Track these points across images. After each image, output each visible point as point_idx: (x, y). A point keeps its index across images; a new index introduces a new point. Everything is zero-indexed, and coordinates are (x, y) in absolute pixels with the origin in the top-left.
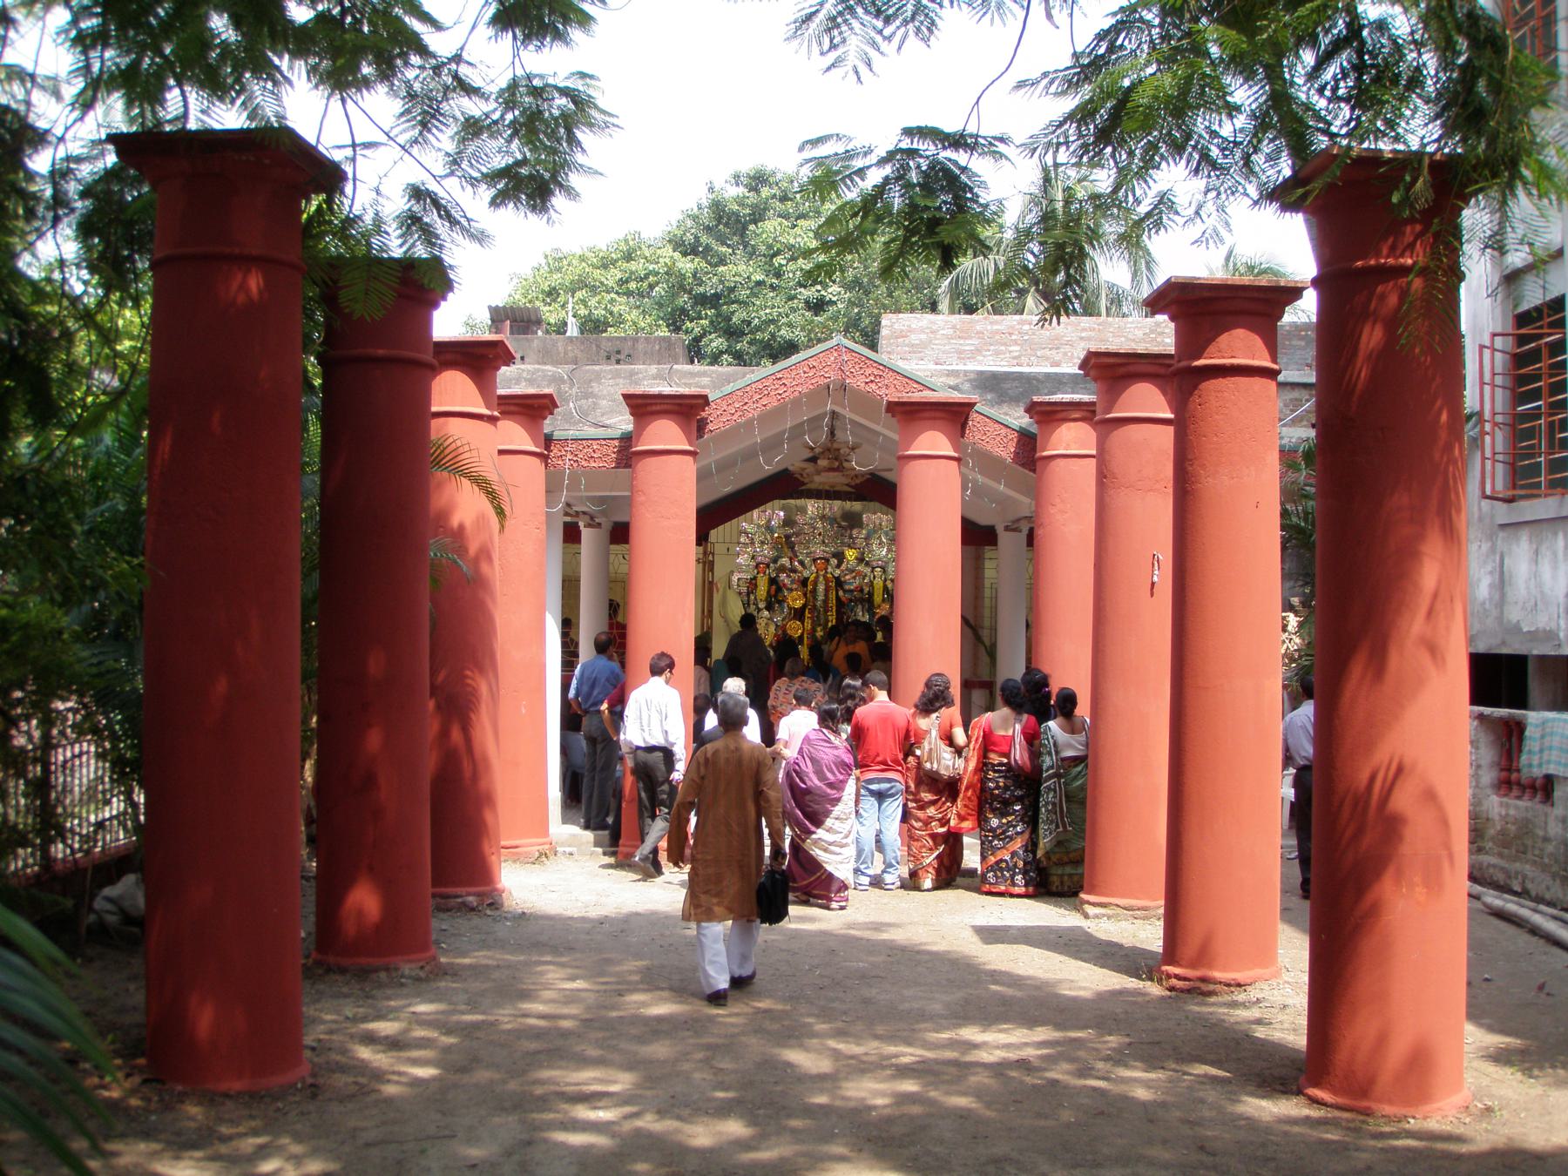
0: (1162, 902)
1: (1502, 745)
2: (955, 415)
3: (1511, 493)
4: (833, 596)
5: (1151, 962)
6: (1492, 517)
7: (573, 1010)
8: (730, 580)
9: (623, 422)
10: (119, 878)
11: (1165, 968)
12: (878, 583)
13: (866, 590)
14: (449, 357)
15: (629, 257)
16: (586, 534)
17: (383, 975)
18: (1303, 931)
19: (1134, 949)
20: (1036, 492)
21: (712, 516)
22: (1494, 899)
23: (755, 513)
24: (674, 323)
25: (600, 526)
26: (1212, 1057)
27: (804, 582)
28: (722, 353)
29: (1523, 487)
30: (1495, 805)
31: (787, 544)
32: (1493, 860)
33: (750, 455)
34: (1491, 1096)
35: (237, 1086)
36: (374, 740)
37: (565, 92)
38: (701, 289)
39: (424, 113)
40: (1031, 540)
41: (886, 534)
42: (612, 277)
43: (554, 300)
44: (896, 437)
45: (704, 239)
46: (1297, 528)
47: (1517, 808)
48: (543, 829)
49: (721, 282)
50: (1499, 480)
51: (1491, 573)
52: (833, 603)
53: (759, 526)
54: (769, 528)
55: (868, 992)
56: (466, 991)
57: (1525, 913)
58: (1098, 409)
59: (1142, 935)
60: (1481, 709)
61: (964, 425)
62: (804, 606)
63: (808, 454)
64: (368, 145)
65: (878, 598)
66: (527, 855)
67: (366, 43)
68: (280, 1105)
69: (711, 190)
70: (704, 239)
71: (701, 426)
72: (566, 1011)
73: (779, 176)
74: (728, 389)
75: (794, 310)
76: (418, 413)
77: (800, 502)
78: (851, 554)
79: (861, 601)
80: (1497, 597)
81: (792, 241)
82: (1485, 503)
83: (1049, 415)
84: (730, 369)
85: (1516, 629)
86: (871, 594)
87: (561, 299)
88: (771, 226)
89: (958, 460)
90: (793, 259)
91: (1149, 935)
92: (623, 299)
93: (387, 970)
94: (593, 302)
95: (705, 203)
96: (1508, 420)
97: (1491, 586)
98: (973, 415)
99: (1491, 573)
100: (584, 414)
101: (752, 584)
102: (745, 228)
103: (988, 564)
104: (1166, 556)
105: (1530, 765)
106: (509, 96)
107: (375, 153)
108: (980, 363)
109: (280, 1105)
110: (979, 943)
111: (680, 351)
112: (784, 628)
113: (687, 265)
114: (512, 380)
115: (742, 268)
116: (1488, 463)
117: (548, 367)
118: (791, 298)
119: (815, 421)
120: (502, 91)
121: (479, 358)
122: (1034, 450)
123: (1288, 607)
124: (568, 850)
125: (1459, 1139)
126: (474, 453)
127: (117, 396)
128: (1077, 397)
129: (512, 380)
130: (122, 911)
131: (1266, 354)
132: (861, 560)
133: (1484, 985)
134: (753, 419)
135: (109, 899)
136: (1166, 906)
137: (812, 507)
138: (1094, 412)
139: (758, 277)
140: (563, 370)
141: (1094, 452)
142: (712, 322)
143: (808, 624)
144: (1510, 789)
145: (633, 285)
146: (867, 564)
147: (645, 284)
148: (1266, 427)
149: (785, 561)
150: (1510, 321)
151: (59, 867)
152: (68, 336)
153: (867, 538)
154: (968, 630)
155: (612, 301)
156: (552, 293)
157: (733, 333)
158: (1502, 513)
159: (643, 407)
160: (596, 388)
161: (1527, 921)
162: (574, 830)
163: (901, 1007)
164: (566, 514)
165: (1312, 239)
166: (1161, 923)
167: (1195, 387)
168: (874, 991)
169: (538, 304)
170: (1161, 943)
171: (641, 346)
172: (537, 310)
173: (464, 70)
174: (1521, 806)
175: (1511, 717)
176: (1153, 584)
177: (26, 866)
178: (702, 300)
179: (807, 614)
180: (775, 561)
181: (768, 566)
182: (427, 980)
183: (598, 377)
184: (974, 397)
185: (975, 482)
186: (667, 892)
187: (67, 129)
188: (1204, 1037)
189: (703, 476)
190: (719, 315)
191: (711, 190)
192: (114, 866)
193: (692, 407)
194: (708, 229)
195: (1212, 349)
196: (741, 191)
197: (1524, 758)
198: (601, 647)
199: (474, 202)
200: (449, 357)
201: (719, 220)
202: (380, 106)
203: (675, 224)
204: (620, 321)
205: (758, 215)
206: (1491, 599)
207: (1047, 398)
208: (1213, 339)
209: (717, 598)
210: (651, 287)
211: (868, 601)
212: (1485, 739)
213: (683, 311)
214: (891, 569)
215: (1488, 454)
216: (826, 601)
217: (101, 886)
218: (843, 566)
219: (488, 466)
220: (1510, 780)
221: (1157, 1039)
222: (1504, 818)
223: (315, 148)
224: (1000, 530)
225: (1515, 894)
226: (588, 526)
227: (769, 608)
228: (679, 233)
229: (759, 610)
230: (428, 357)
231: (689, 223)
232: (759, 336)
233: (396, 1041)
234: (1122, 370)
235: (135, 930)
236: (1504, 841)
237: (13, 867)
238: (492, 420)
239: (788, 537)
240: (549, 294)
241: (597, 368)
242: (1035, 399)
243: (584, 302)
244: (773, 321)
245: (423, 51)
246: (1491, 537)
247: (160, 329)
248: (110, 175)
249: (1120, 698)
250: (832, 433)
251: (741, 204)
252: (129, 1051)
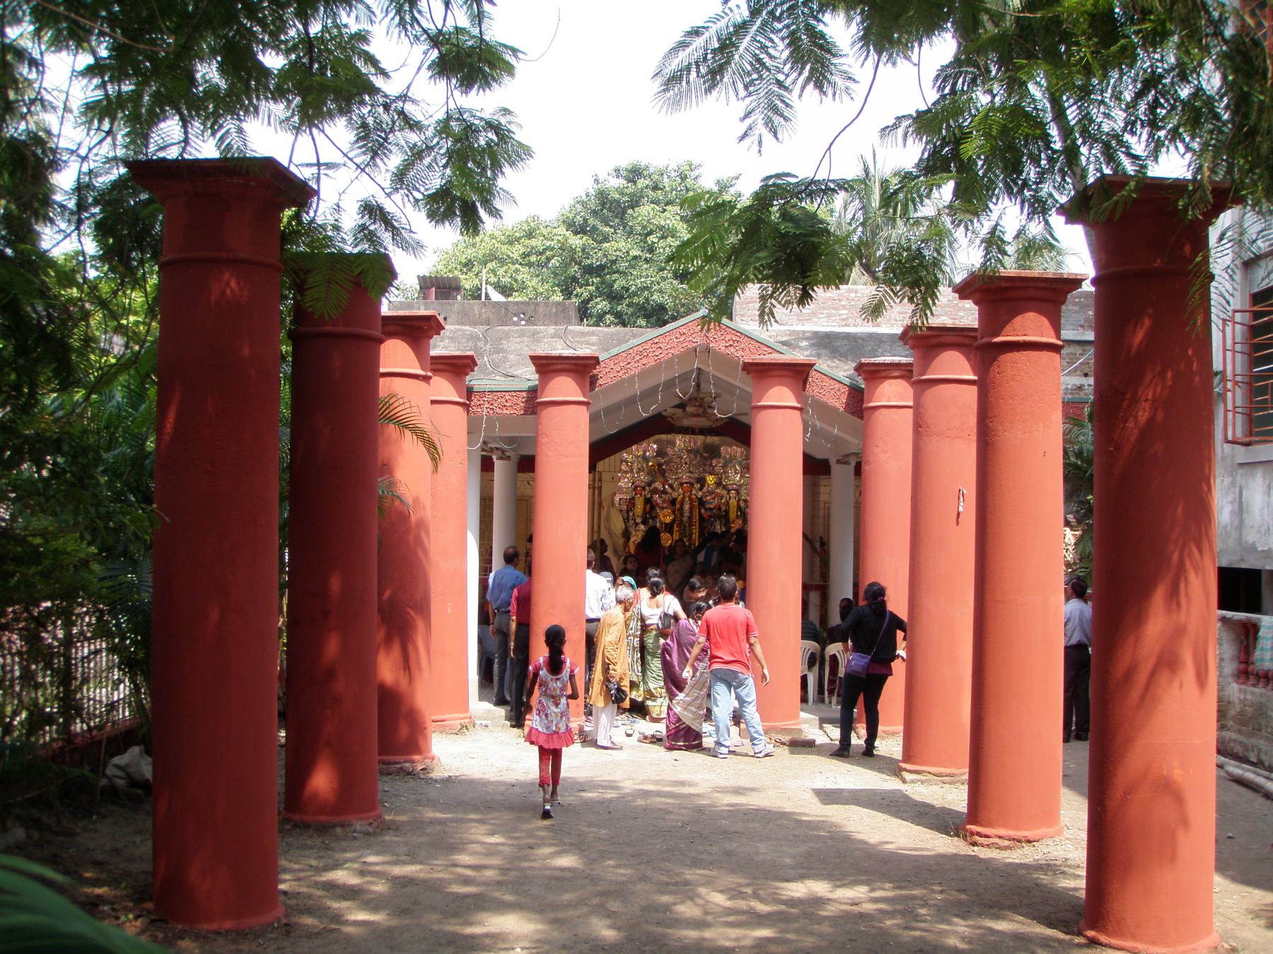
0: (967, 770)
1: (1241, 642)
2: (798, 374)
3: (1248, 439)
4: (696, 513)
5: (957, 821)
6: (1233, 457)
7: (494, 861)
8: (613, 501)
9: (529, 375)
10: (125, 750)
11: (969, 827)
12: (733, 502)
13: (723, 508)
14: (392, 328)
15: (530, 235)
16: (498, 465)
17: (339, 830)
18: (1082, 794)
19: (943, 809)
20: (864, 435)
21: (601, 450)
22: (1235, 769)
23: (634, 447)
24: (567, 288)
25: (511, 461)
26: (1009, 903)
27: (673, 502)
28: (605, 313)
29: (1258, 434)
30: (1235, 690)
31: (659, 471)
32: (1234, 736)
33: (631, 401)
34: (1235, 938)
35: (228, 924)
36: (332, 646)
37: (490, 125)
38: (589, 261)
39: (372, 142)
40: (858, 470)
41: (740, 464)
42: (517, 251)
43: (470, 270)
44: (750, 390)
45: (592, 221)
46: (1075, 466)
47: (1252, 693)
48: (465, 708)
49: (605, 256)
50: (1237, 427)
51: (1231, 502)
52: (696, 518)
53: (638, 457)
54: (644, 457)
55: (732, 846)
56: (406, 844)
57: (1260, 780)
58: (915, 370)
59: (950, 797)
60: (1224, 612)
61: (805, 382)
62: (673, 521)
63: (677, 402)
64: (330, 166)
65: (732, 515)
66: (451, 727)
67: (330, 84)
68: (261, 941)
69: (597, 181)
70: (592, 221)
71: (593, 381)
72: (487, 862)
73: (652, 170)
74: (615, 351)
75: (664, 279)
76: (369, 374)
77: (670, 437)
78: (711, 479)
79: (720, 517)
80: (1237, 522)
81: (663, 223)
82: (1226, 446)
83: (874, 373)
84: (613, 329)
85: (1252, 549)
86: (727, 512)
87: (476, 269)
88: (645, 210)
89: (800, 409)
90: (663, 237)
91: (956, 798)
92: (526, 269)
93: (342, 826)
94: (501, 272)
95: (592, 192)
96: (1246, 380)
97: (1232, 513)
98: (813, 373)
99: (1231, 502)
100: (496, 366)
101: (631, 503)
102: (624, 212)
103: (822, 490)
104: (970, 491)
105: (1262, 660)
106: (444, 128)
107: (339, 176)
108: (815, 324)
109: (261, 941)
110: (819, 804)
111: (573, 314)
113: (576, 241)
114: (440, 347)
115: (622, 244)
116: (1230, 415)
117: (467, 328)
118: (662, 269)
119: (684, 377)
120: (439, 122)
121: (417, 330)
122: (862, 401)
123: (1067, 524)
124: (484, 722)
126: (414, 410)
127: (124, 365)
128: (897, 359)
129: (440, 347)
130: (129, 777)
131: (1052, 332)
132: (719, 484)
133: (1228, 842)
134: (634, 376)
135: (117, 766)
136: (970, 773)
137: (680, 441)
138: (911, 371)
139: (635, 252)
140: (478, 330)
141: (911, 404)
142: (597, 288)
144: (1248, 678)
145: (533, 259)
146: (724, 487)
147: (543, 258)
148: (1052, 384)
149: (658, 485)
150: (1248, 299)
151: (78, 740)
152: (86, 315)
153: (724, 466)
154: (808, 545)
155: (517, 271)
156: (468, 265)
157: (614, 297)
158: (1241, 454)
159: (547, 366)
160: (505, 344)
161: (1262, 787)
162: (488, 706)
163: (756, 859)
164: (483, 450)
165: (1090, 245)
166: (966, 787)
167: (995, 359)
168: (734, 845)
169: (456, 273)
170: (965, 804)
171: (541, 309)
172: (456, 279)
173: (409, 108)
174: (1255, 693)
175: (1249, 620)
176: (959, 514)
177: (52, 740)
178: (590, 270)
180: (649, 484)
181: (644, 488)
182: (374, 834)
183: (507, 336)
184: (813, 359)
185: (814, 426)
187: (90, 150)
188: (1001, 885)
189: (594, 419)
190: (603, 282)
191: (597, 181)
192: (122, 739)
193: (586, 366)
194: (594, 213)
195: (1008, 328)
196: (621, 182)
197: (1257, 653)
198: (510, 559)
199: (416, 220)
200: (392, 328)
201: (603, 205)
202: (340, 132)
203: (567, 208)
204: (523, 287)
205: (635, 203)
206: (1232, 524)
207: (872, 360)
208: (1009, 321)
209: (604, 513)
210: (548, 259)
211: (724, 517)
212: (1227, 637)
213: (574, 279)
214: (743, 491)
215: (1230, 407)
216: (690, 518)
217: (112, 756)
218: (705, 489)
219: (424, 416)
220: (1246, 672)
221: (963, 887)
222: (1243, 701)
223: (287, 170)
224: (833, 463)
225: (1252, 764)
226: (500, 458)
228: (571, 216)
229: (637, 524)
230: (377, 333)
231: (579, 207)
232: (635, 300)
233: (350, 881)
234: (935, 341)
235: (139, 791)
236: (1242, 720)
237: (42, 741)
238: (426, 379)
239: (660, 465)
240: (466, 265)
241: (506, 328)
242: (863, 360)
243: (494, 272)
244: (647, 288)
245: (373, 90)
246: (1232, 474)
247: (159, 305)
248: (118, 185)
249: (932, 604)
250: (698, 385)
251: (622, 194)
252: (139, 896)
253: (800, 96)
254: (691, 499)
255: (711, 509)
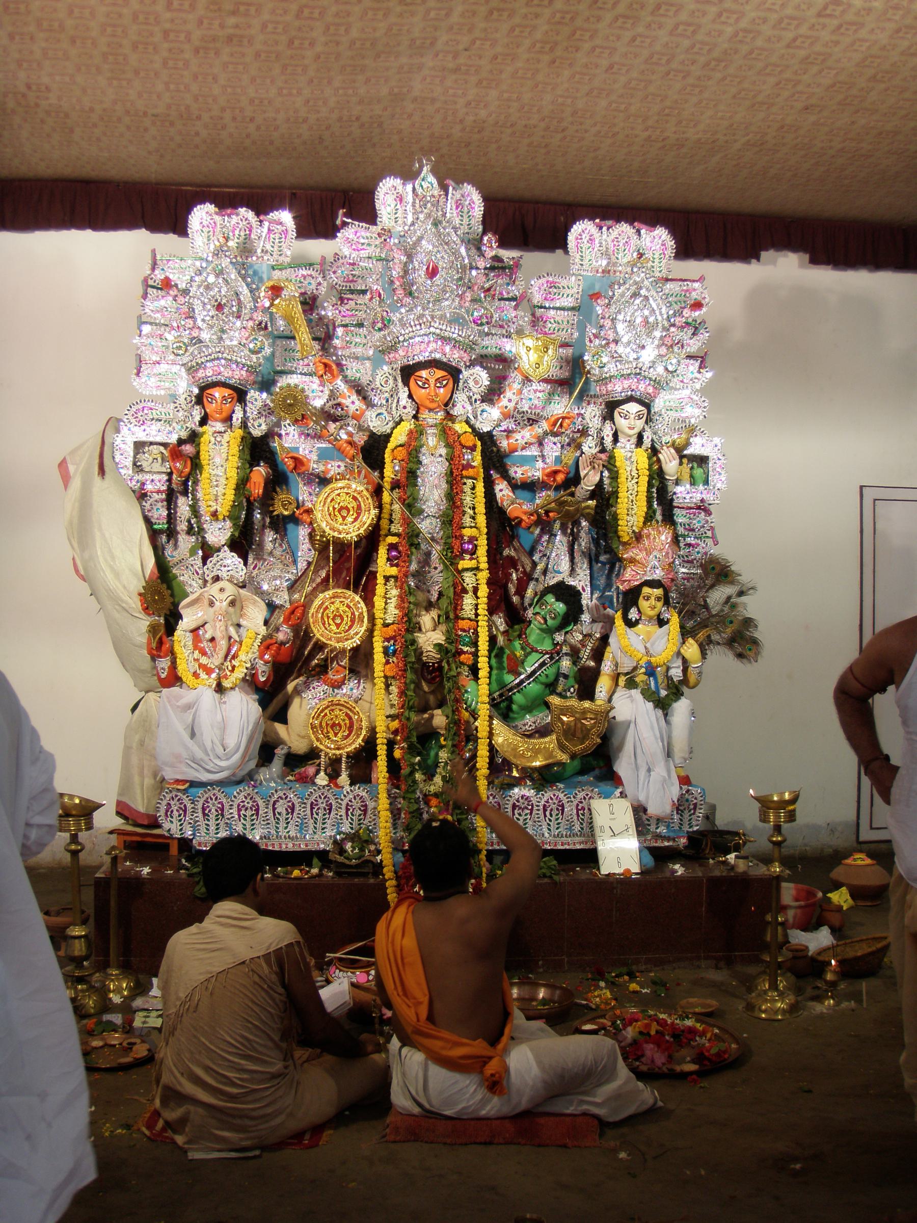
4: (474, 497)
12: (632, 462)
27: (373, 451)
52: (476, 526)
62: (372, 538)
86: (604, 498)
101: (186, 456)
112: (298, 618)
125: (71, 523)
132: (572, 378)
143: (388, 603)
179: (383, 566)
181: (240, 395)
186: (155, 981)
218: (509, 398)
227: (242, 544)
229: (208, 551)
253: (74, 559)
254: (445, 432)
255: (530, 487)
